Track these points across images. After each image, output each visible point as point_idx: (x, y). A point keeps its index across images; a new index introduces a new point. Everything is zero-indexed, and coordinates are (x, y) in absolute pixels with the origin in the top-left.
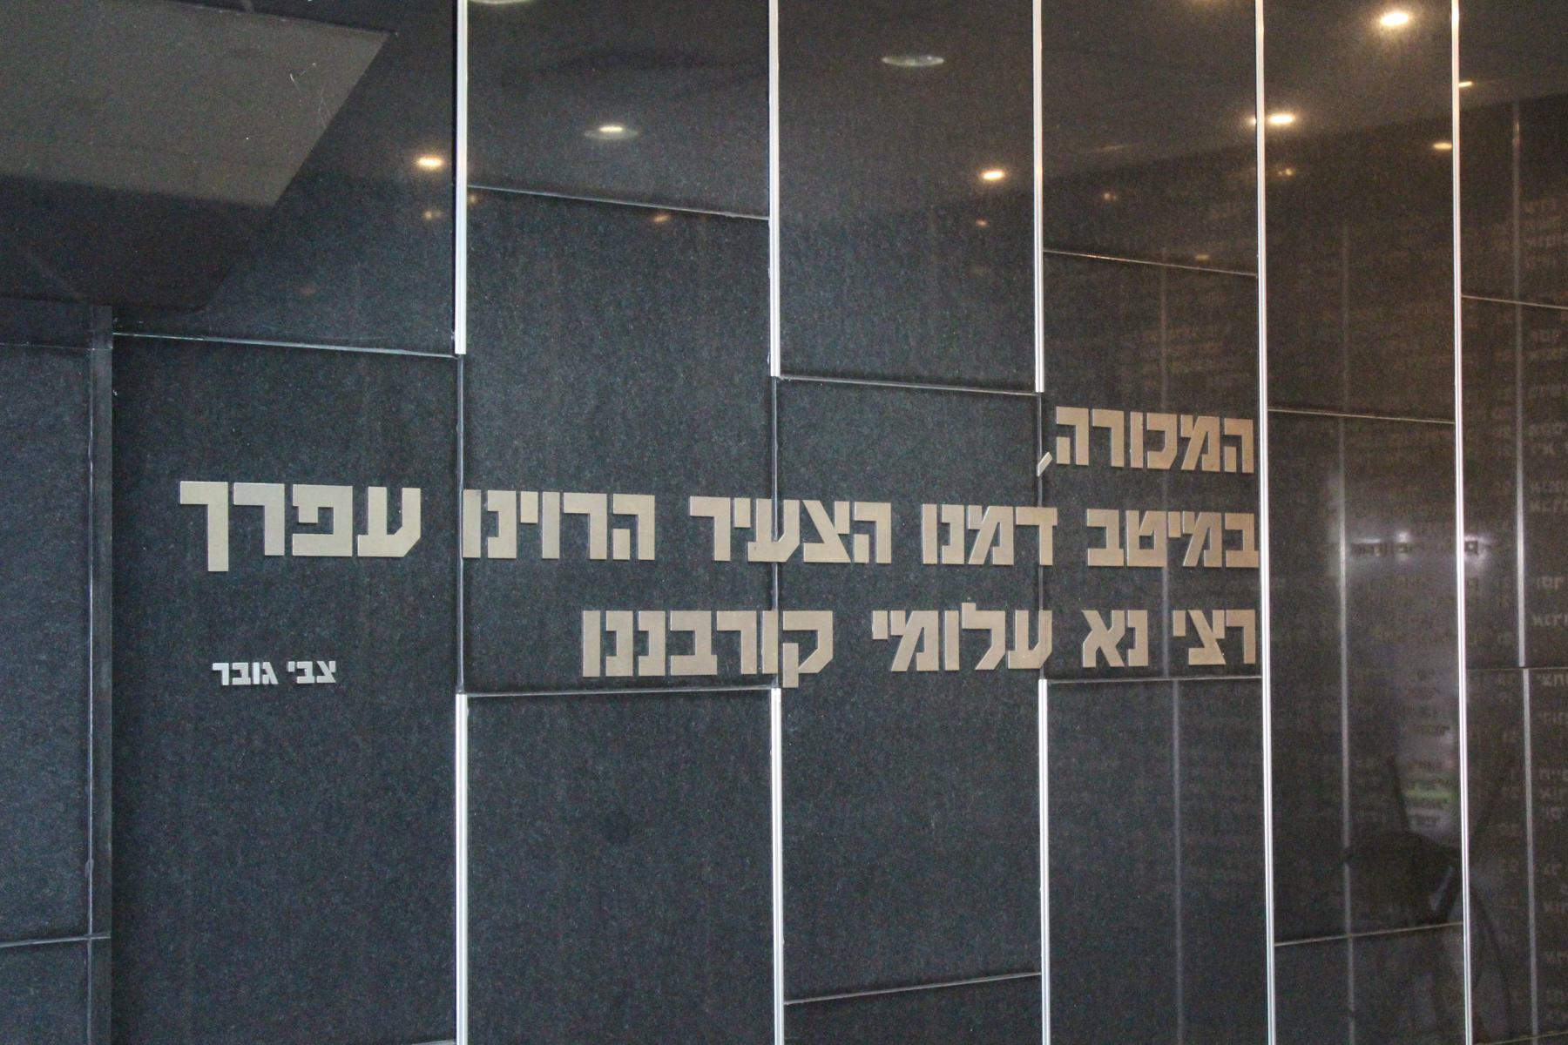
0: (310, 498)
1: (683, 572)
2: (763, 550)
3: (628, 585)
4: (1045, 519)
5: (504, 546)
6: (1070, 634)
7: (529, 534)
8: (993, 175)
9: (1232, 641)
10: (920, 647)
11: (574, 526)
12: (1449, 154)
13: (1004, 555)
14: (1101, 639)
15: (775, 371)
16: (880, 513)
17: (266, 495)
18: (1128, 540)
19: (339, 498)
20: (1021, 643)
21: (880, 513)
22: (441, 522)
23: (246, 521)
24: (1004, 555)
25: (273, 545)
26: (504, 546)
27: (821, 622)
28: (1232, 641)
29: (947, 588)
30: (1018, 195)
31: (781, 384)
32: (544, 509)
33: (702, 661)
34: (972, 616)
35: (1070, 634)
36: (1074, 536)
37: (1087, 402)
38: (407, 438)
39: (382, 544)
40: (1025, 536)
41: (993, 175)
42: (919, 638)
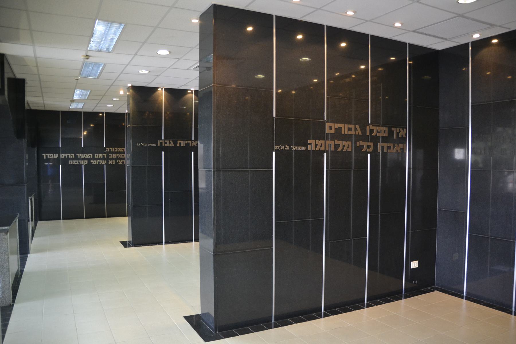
0: (50, 155)
1: (76, 158)
2: (82, 157)
3: (73, 159)
4: (105, 155)
5: (63, 157)
6: (107, 162)
7: (65, 156)
8: (363, 67)
9: (123, 162)
10: (321, 146)
11: (68, 156)
12: (409, 61)
13: (102, 157)
14: (110, 162)
15: (274, 116)
16: (91, 155)
17: (48, 155)
18: (112, 156)
19: (52, 155)
20: (104, 163)
21: (91, 155)
22: (59, 156)
23: (47, 156)
24: (102, 157)
25: (163, 145)
26: (63, 157)
27: (87, 161)
28: (123, 162)
29: (97, 159)
30: (366, 70)
31: (276, 119)
32: (66, 155)
33: (78, 163)
34: (336, 142)
35: (107, 162)
36: (108, 156)
37: (109, 147)
38: (56, 150)
39: (55, 157)
40: (103, 156)
41: (363, 67)
42: (94, 162)
